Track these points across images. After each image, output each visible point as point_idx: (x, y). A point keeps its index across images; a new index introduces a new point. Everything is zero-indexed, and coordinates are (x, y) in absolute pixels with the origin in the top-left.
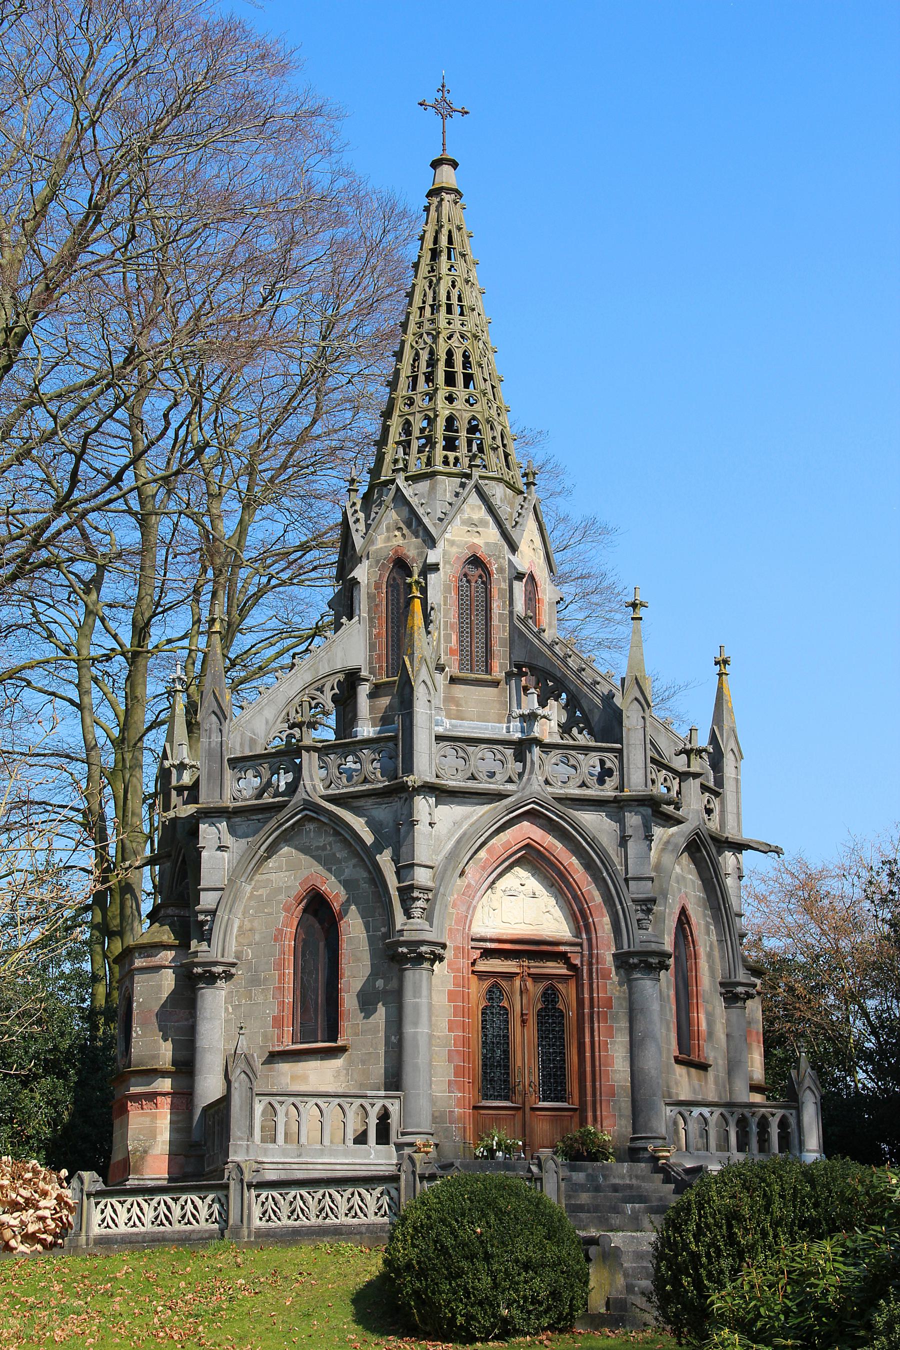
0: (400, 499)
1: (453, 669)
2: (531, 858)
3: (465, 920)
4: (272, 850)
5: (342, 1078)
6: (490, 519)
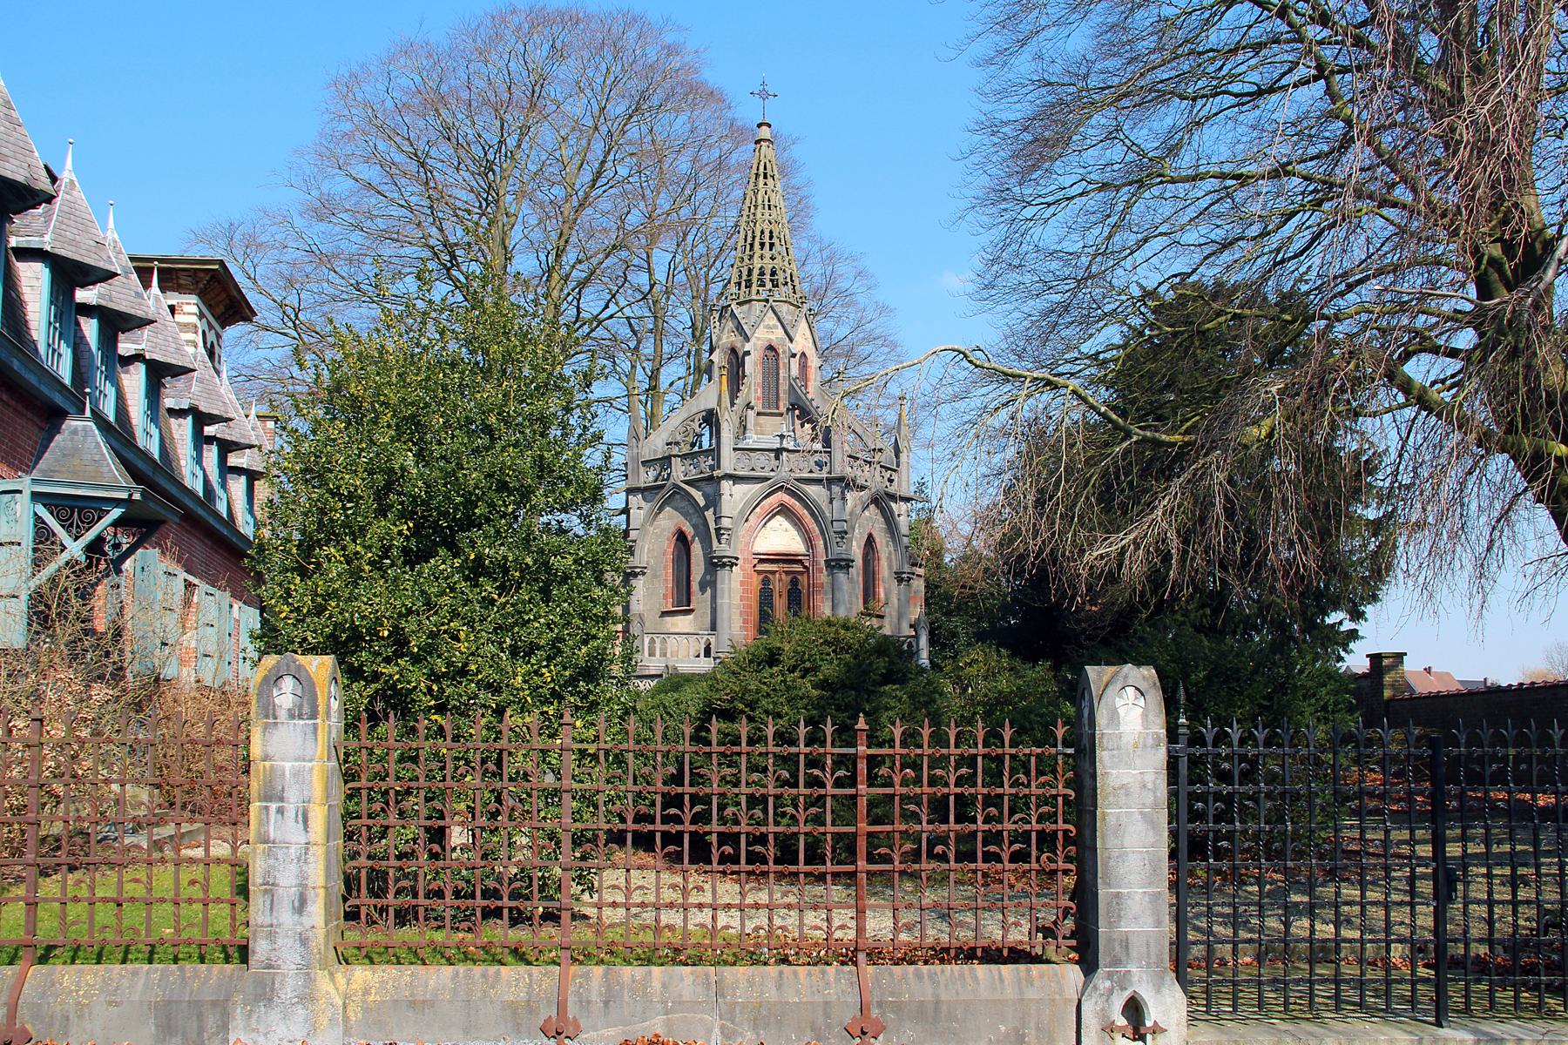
0: (733, 314)
1: (759, 408)
2: (784, 510)
4: (661, 509)
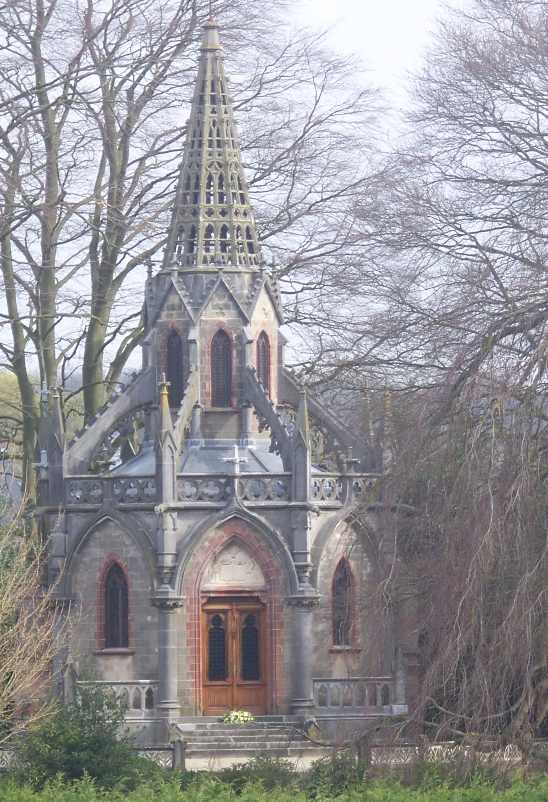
3: (199, 580)
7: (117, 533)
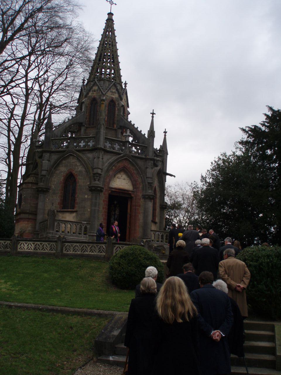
5: (75, 218)
6: (117, 92)
7: (74, 161)
